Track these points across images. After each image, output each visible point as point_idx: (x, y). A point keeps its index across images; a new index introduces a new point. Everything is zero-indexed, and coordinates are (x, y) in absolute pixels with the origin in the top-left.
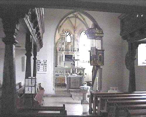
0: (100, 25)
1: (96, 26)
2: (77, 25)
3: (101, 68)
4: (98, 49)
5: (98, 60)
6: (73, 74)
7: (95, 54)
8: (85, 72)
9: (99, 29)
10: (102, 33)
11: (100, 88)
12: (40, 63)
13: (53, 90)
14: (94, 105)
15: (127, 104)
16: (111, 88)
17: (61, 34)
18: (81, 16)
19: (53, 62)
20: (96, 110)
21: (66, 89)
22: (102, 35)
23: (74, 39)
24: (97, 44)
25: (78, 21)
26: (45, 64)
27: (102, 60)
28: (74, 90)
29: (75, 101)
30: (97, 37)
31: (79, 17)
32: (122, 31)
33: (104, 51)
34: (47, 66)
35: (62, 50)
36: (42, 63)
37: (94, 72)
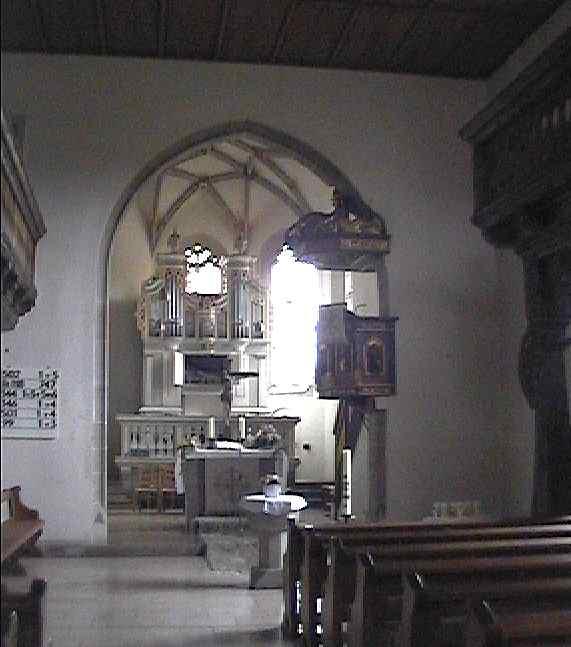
0: (372, 196)
1: (347, 200)
2: (252, 216)
3: (378, 407)
4: (360, 313)
5: (362, 368)
6: (220, 444)
7: (341, 335)
8: (301, 433)
9: (367, 214)
10: (384, 236)
11: (380, 508)
12: (20, 384)
13: (99, 519)
14: (307, 590)
15: (513, 574)
16: (436, 505)
17: (164, 257)
18: (273, 166)
19: (95, 383)
20: (315, 619)
21: (182, 520)
22: (383, 246)
23: (233, 278)
24: (356, 291)
25: (257, 190)
26: (48, 389)
27: (383, 367)
28: (223, 520)
29: (219, 575)
30: (353, 254)
31: (267, 173)
32: (485, 193)
33: (397, 324)
34: (58, 402)
35: (172, 334)
36: (36, 385)
37: (346, 431)
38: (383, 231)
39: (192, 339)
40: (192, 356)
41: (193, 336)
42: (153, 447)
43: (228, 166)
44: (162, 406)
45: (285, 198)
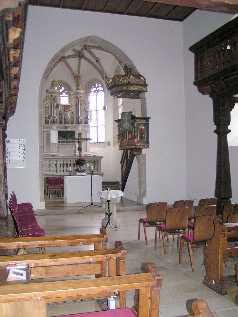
22: (143, 88)
35: (54, 122)
38: (145, 83)
39: (73, 125)
40: (63, 132)
41: (48, 123)
42: (48, 169)
43: (74, 53)
44: (50, 152)
45: (95, 66)
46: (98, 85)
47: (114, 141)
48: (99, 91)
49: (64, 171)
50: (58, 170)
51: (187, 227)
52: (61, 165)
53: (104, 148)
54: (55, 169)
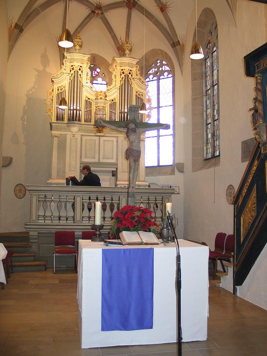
45: (157, 23)
46: (161, 62)
47: (194, 161)
48: (162, 73)
49: (106, 220)
50: (78, 217)
51: (70, 179)
52: (83, 205)
53: (173, 176)
54: (72, 214)
